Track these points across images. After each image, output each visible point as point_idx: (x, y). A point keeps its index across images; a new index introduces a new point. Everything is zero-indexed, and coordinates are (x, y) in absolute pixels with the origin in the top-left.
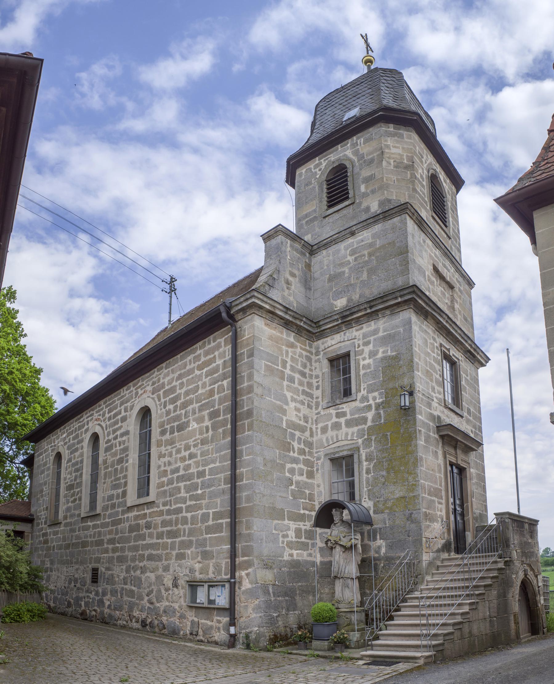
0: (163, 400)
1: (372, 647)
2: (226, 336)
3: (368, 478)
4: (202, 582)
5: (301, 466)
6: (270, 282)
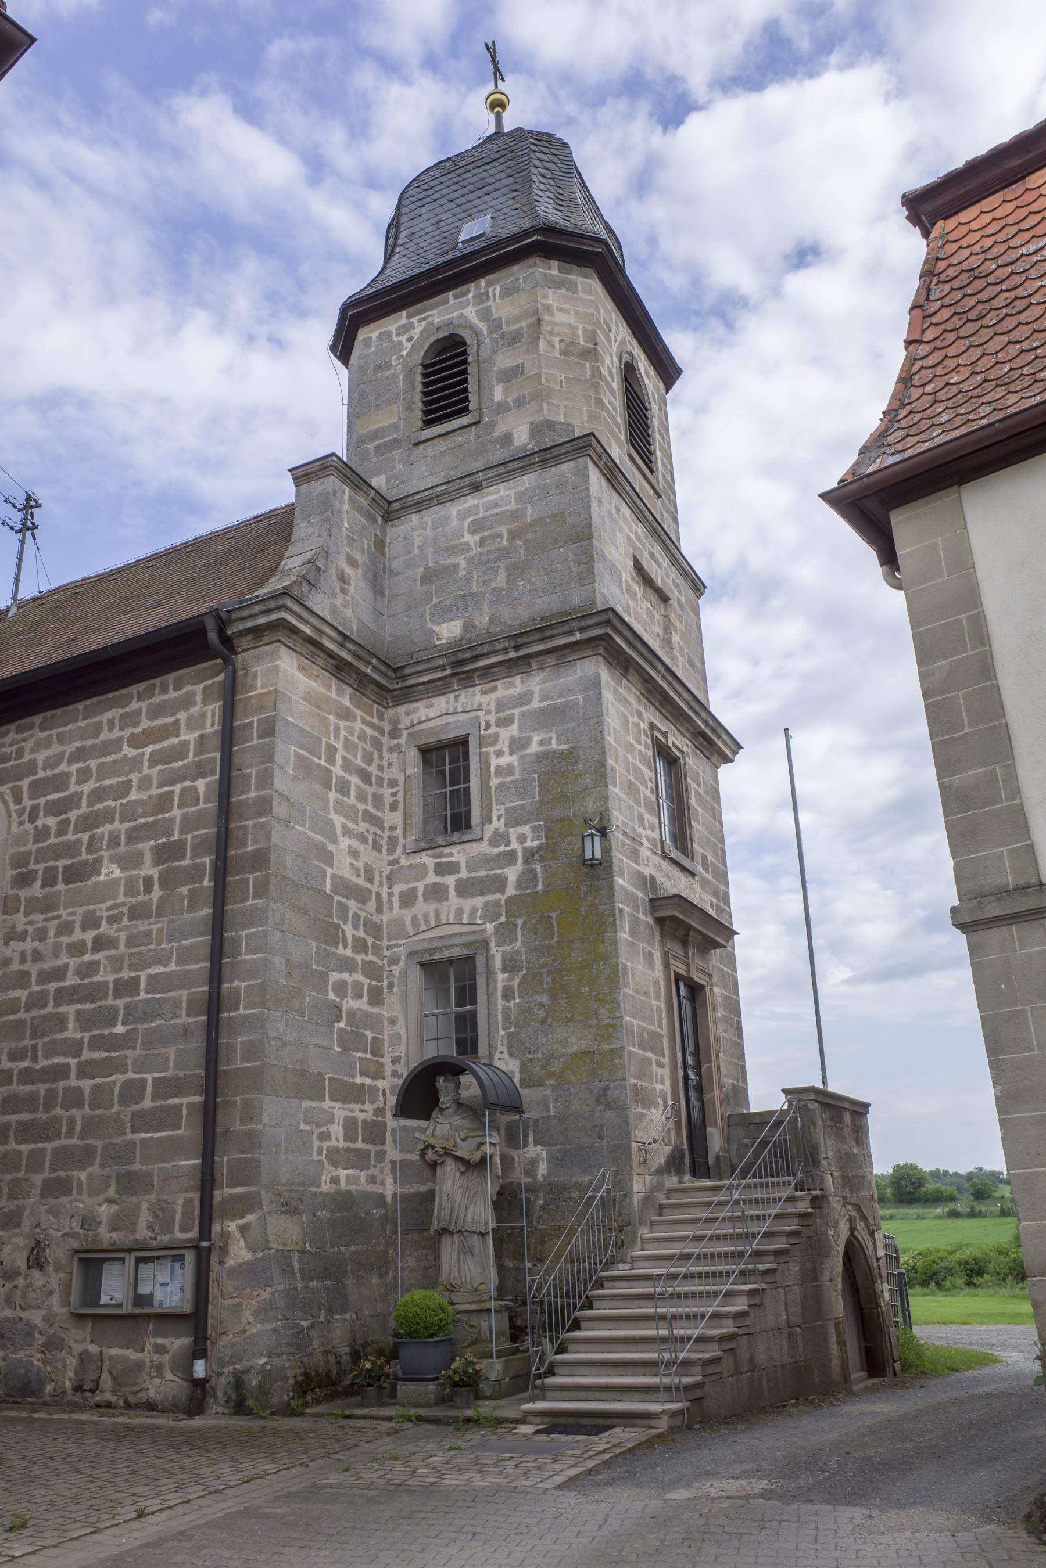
0: (27, 803)
1: (543, 1393)
2: (209, 682)
3: (508, 1008)
4: (116, 1253)
5: (359, 977)
6: (311, 577)
